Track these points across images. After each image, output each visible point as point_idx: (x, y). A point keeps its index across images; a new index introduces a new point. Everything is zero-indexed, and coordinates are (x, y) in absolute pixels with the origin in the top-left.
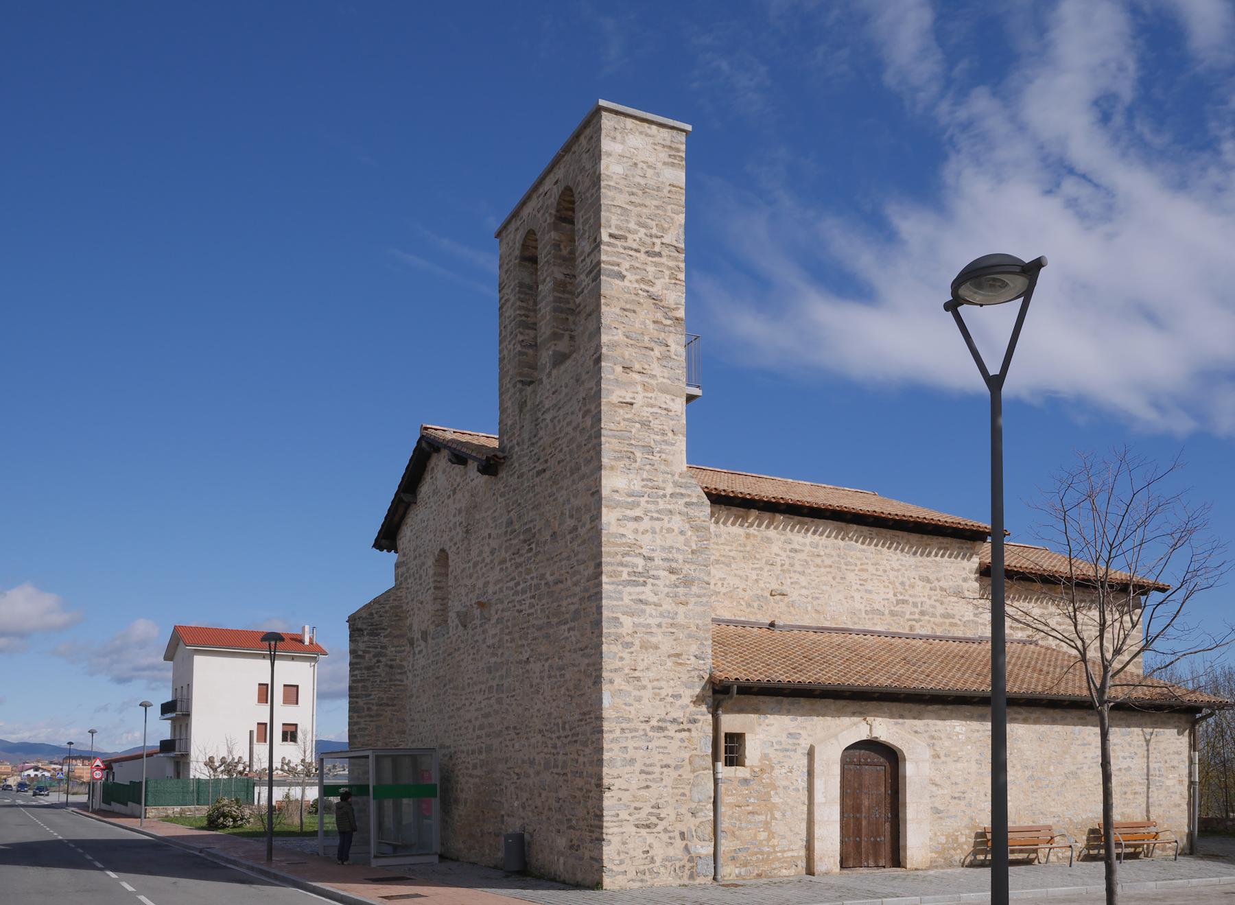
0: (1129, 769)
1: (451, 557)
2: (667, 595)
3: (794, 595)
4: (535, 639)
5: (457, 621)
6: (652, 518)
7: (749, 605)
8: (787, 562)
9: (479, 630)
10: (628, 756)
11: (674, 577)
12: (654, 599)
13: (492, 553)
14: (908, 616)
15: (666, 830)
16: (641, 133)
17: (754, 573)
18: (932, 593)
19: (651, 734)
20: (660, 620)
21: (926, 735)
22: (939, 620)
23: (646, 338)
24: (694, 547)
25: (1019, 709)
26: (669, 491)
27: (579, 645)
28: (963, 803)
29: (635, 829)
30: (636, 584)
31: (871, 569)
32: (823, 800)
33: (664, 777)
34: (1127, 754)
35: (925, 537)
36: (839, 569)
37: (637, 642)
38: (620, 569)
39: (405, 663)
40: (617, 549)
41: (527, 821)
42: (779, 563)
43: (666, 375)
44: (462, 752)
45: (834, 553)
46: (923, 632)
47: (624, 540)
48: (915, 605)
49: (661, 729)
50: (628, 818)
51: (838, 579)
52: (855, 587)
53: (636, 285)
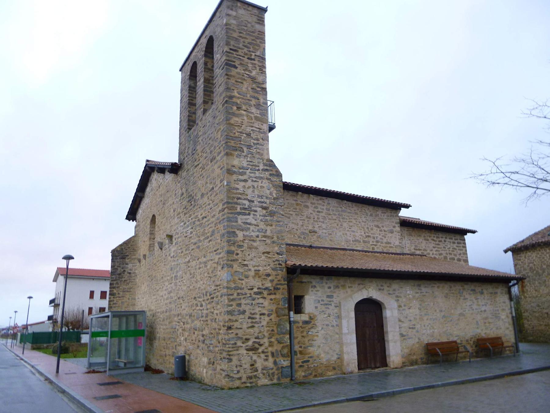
0: (485, 311)
1: (157, 217)
2: (261, 221)
3: (320, 232)
4: (192, 250)
5: (158, 247)
6: (252, 181)
7: (299, 237)
8: (316, 217)
9: (168, 250)
10: (241, 309)
11: (264, 211)
12: (254, 222)
13: (174, 211)
14: (371, 243)
15: (263, 352)
16: (244, 9)
17: (301, 222)
18: (381, 232)
19: (254, 296)
20: (258, 233)
21: (394, 295)
22: (384, 245)
23: (248, 96)
24: (275, 196)
25: (436, 282)
26: (261, 167)
27: (214, 249)
28: (414, 330)
29: (245, 352)
30: (245, 214)
31: (354, 221)
32: (347, 331)
33: (262, 320)
34: (483, 304)
35: (376, 208)
36: (339, 220)
37: (246, 245)
38: (236, 206)
39: (136, 271)
40: (235, 196)
41: (187, 348)
42: (312, 217)
43: (258, 112)
44: (158, 312)
45: (337, 213)
46: (378, 250)
47: (238, 191)
48: (374, 238)
49: (260, 293)
50: (242, 345)
51: (339, 225)
52: (347, 229)
53: (243, 72)
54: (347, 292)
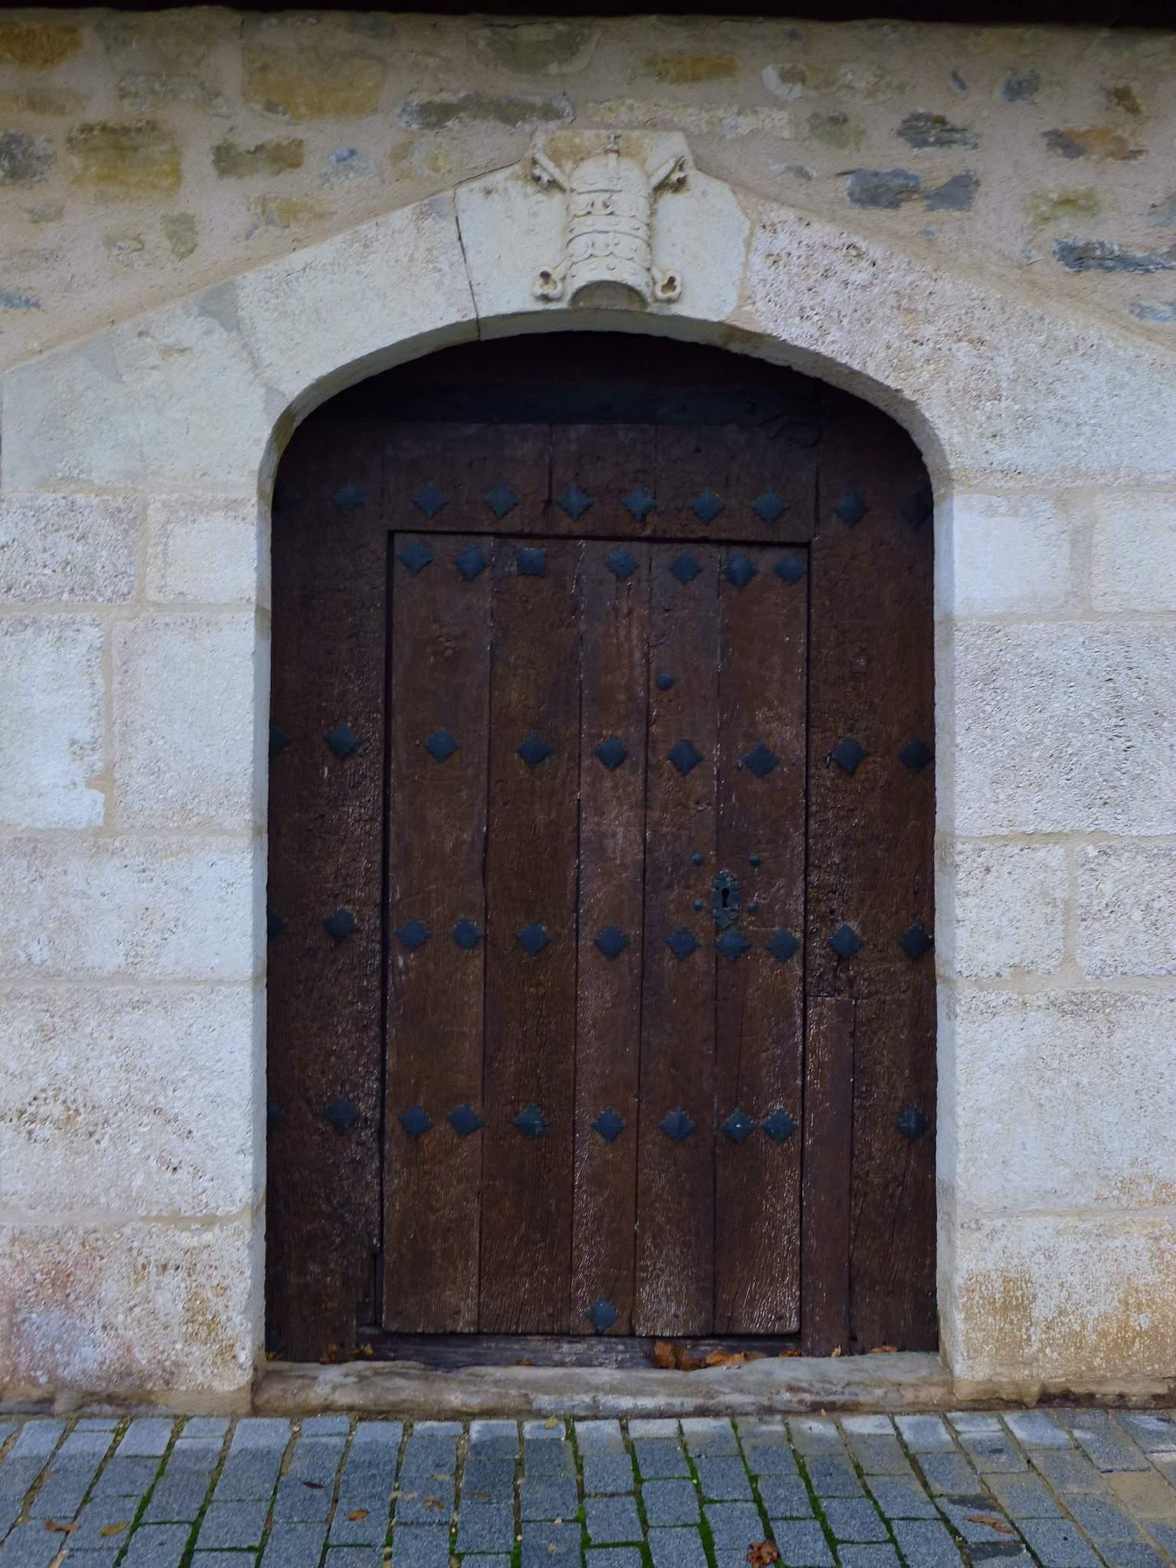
32: (86, 807)
54: (183, 233)
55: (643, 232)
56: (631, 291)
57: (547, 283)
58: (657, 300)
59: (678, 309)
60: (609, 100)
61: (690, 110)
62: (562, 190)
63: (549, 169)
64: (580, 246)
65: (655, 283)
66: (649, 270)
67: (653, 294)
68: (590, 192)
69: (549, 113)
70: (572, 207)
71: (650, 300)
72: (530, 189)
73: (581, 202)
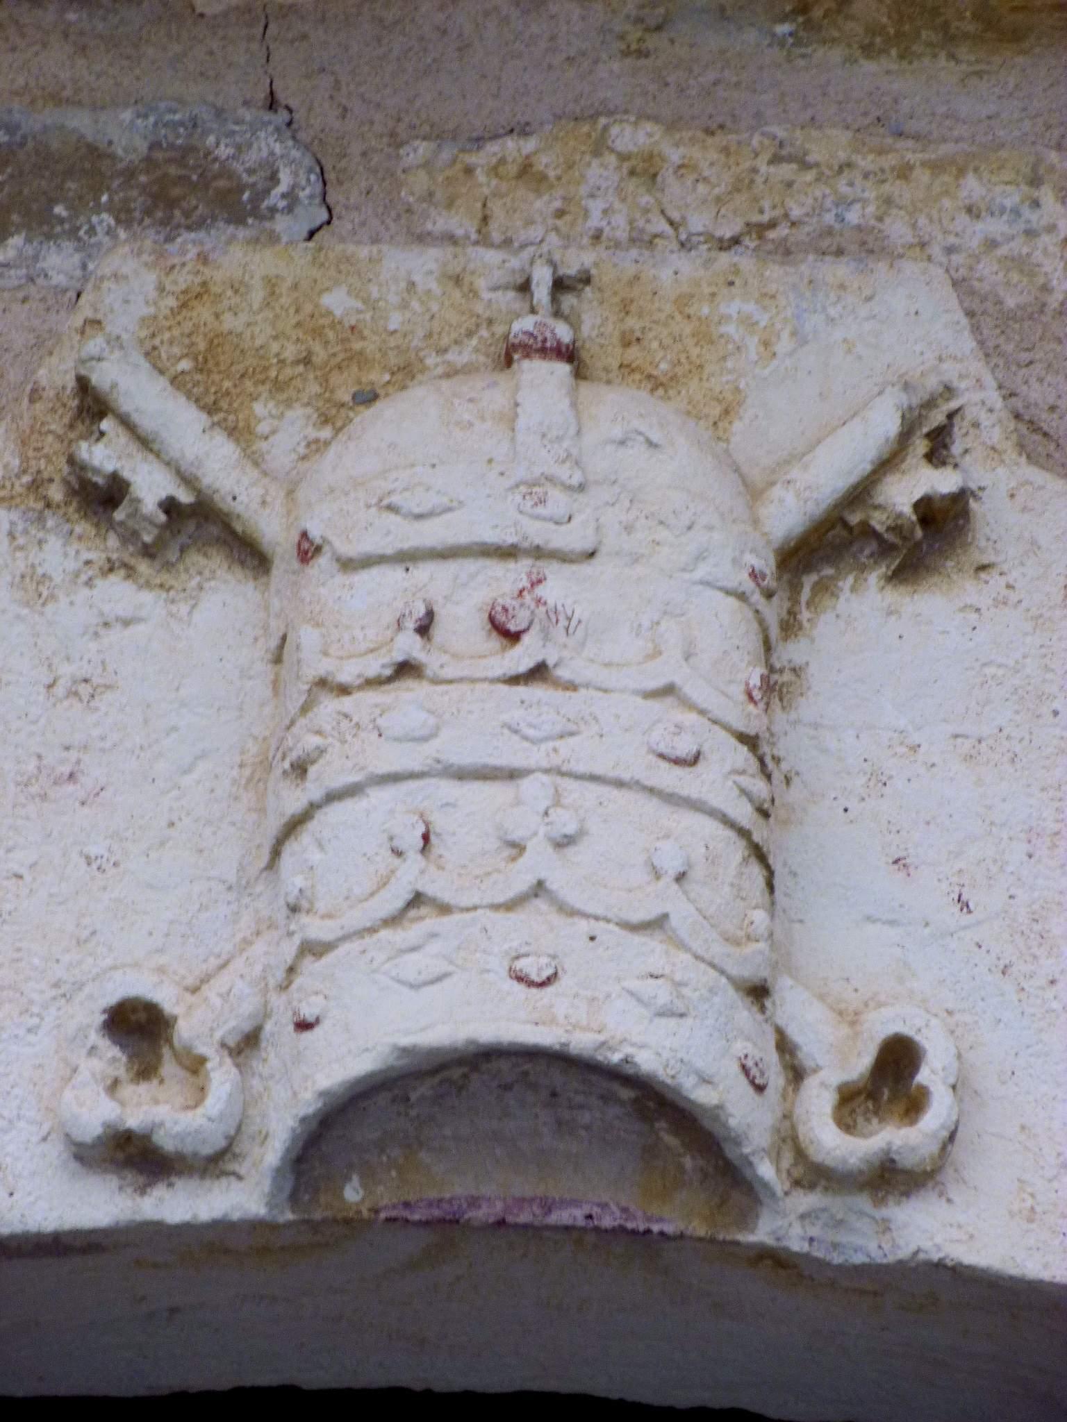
55: (723, 778)
56: (654, 1111)
57: (145, 1071)
58: (815, 1175)
59: (927, 1230)
60: (523, 130)
61: (972, 187)
62: (250, 554)
63: (172, 442)
64: (346, 857)
65: (797, 1075)
66: (758, 993)
67: (789, 1139)
68: (407, 558)
69: (182, 192)
70: (308, 637)
71: (766, 1170)
72: (63, 551)
73: (355, 616)
